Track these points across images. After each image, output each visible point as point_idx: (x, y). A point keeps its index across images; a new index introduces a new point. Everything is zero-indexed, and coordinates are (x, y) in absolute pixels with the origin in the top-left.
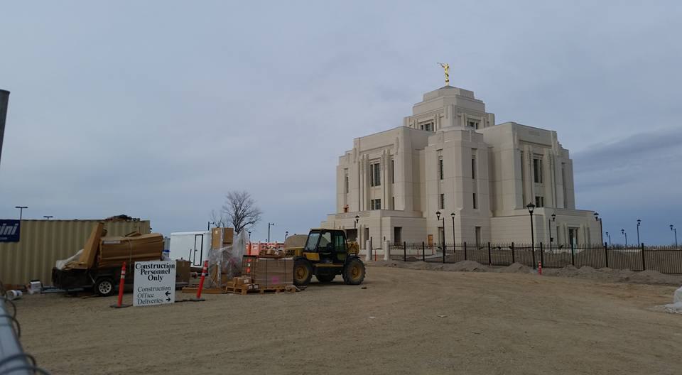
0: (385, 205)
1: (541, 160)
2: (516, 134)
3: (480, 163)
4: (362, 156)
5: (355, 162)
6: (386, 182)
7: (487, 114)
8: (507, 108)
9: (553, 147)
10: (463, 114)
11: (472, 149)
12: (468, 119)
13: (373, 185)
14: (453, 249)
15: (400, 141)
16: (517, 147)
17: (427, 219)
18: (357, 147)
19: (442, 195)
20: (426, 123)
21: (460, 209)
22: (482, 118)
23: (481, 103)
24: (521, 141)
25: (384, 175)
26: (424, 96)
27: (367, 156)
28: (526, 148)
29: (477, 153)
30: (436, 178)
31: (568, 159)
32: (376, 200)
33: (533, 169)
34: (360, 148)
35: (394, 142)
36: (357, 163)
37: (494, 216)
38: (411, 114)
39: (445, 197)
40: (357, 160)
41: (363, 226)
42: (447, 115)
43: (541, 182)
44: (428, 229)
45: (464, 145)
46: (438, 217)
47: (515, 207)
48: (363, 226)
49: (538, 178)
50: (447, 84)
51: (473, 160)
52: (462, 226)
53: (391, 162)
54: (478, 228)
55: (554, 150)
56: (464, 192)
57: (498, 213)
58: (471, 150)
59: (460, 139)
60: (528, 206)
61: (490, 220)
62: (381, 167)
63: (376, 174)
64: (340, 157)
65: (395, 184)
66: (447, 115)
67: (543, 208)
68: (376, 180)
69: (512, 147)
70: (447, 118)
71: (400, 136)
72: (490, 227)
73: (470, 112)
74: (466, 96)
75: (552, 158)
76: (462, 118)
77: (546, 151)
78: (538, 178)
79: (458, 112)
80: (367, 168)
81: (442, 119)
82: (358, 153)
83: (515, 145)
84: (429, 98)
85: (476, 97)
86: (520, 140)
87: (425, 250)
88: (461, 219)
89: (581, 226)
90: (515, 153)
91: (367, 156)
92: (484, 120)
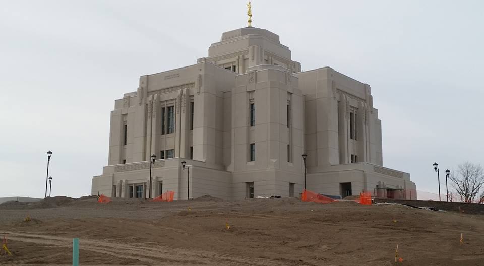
4: (151, 96)
5: (140, 104)
6: (154, 132)
11: (288, 92)
13: (163, 133)
18: (144, 85)
19: (252, 145)
25: (180, 120)
27: (159, 97)
32: (167, 151)
33: (349, 121)
35: (195, 80)
36: (143, 106)
39: (256, 147)
40: (143, 102)
41: (124, 181)
46: (184, 166)
48: (124, 181)
53: (190, 105)
60: (152, 156)
62: (176, 111)
63: (169, 119)
67: (292, 164)
70: (253, 60)
81: (246, 61)
85: (283, 42)
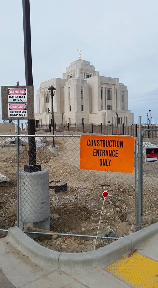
0: (113, 108)
1: (113, 92)
2: (99, 80)
3: (84, 93)
7: (95, 71)
8: (104, 67)
9: (117, 85)
10: (84, 72)
11: (81, 87)
12: (86, 73)
14: (75, 126)
15: (55, 83)
16: (100, 86)
17: (66, 116)
18: (41, 86)
20: (71, 76)
21: (76, 111)
22: (93, 74)
23: (93, 67)
24: (102, 83)
26: (70, 63)
27: (44, 90)
28: (104, 86)
29: (83, 89)
30: (68, 99)
31: (126, 90)
34: (42, 87)
37: (91, 113)
38: (65, 72)
42: (77, 72)
43: (111, 100)
44: (66, 119)
45: (77, 86)
47: (98, 110)
49: (109, 98)
50: (80, 58)
51: (102, 90)
52: (76, 118)
54: (70, 119)
55: (117, 87)
56: (77, 105)
57: (93, 112)
58: (81, 87)
59: (76, 83)
61: (89, 116)
64: (38, 91)
65: (71, 100)
66: (77, 72)
68: (109, 97)
69: (98, 86)
71: (55, 82)
72: (89, 118)
73: (87, 70)
74: (86, 64)
75: (116, 90)
76: (84, 73)
77: (113, 87)
78: (109, 98)
79: (81, 70)
80: (44, 96)
82: (41, 89)
83: (98, 85)
84: (72, 65)
86: (101, 83)
87: (75, 126)
88: (76, 115)
89: (123, 117)
90: (99, 88)
91: (44, 90)
92: (94, 74)
